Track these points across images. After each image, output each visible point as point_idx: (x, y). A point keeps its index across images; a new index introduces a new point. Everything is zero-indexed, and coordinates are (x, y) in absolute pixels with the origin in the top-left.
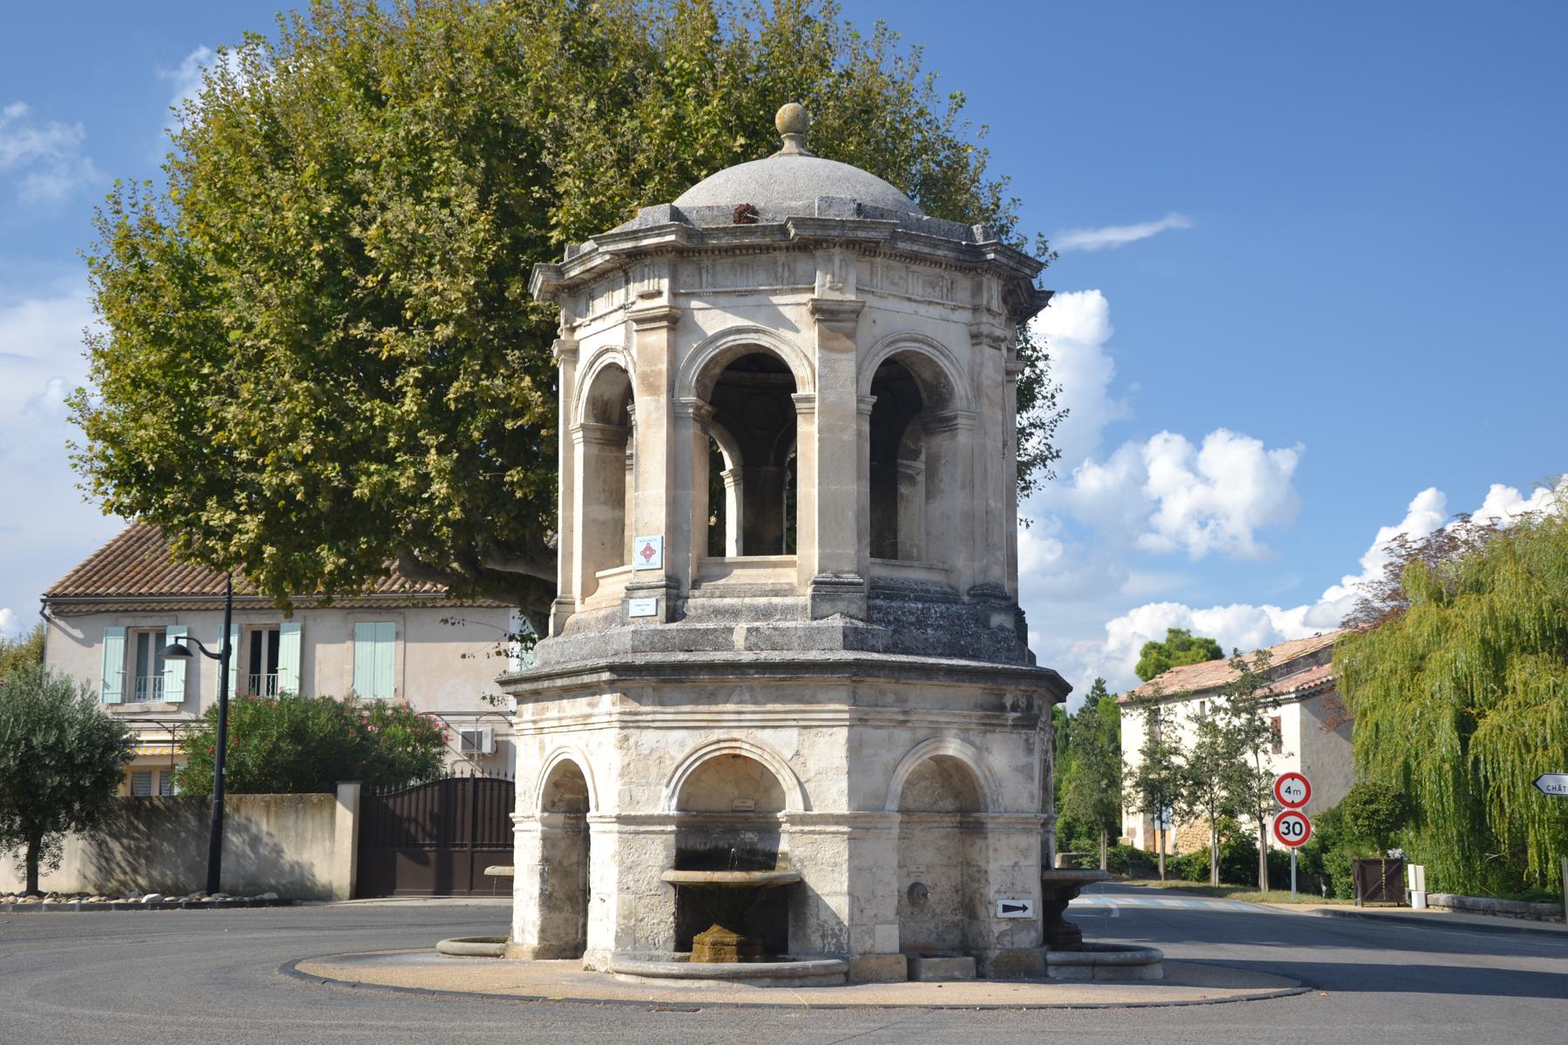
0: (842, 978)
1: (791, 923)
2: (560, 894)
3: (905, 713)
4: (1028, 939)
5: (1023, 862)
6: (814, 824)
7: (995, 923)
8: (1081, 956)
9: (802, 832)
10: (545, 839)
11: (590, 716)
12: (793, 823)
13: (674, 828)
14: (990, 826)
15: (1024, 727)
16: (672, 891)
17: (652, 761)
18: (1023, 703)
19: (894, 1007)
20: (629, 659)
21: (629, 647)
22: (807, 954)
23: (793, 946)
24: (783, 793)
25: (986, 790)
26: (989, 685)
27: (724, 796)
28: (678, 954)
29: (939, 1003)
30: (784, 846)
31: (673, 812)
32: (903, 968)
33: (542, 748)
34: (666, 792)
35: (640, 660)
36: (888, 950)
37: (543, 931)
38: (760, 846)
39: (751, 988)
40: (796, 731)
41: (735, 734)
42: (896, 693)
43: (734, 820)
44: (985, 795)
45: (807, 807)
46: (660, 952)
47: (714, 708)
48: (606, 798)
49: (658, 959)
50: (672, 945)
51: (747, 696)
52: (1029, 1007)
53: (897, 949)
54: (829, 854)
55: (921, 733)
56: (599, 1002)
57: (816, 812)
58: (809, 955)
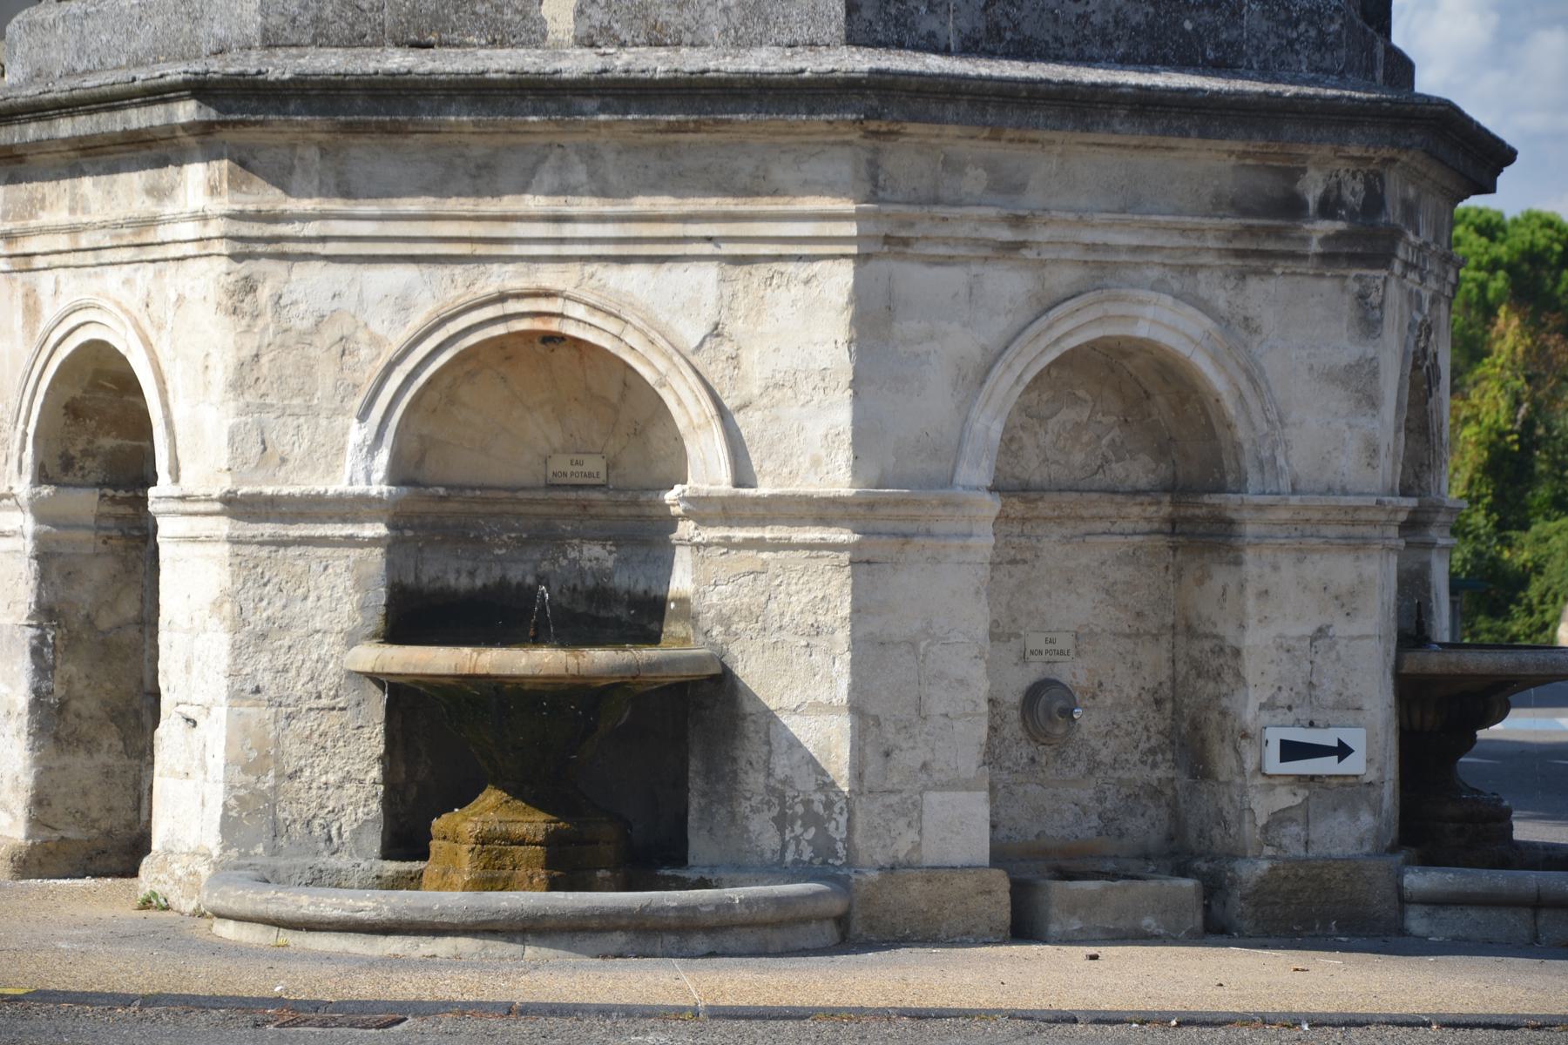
0: (830, 932)
1: (696, 783)
2: (88, 705)
3: (1017, 221)
4: (1349, 834)
5: (1341, 628)
6: (761, 522)
7: (1260, 792)
8: (1501, 880)
9: (728, 544)
10: (45, 556)
11: (152, 222)
12: (702, 521)
13: (380, 530)
14: (1250, 529)
15: (1354, 259)
16: (377, 702)
17: (320, 350)
18: (1354, 192)
19: (941, 1014)
20: (250, 64)
21: (253, 30)
22: (739, 867)
23: (700, 846)
24: (678, 439)
25: (1242, 433)
26: (1257, 144)
27: (521, 446)
28: (392, 867)
29: (1067, 1005)
30: (681, 581)
31: (378, 487)
32: (1000, 906)
33: (32, 310)
34: (358, 434)
35: (281, 67)
36: (958, 857)
37: (40, 801)
38: (622, 581)
39: (572, 959)
40: (711, 271)
41: (548, 277)
42: (991, 167)
43: (555, 511)
44: (1237, 446)
45: (742, 474)
46: (343, 861)
47: (489, 206)
48: (197, 443)
49: (337, 881)
50: (374, 842)
51: (579, 174)
52: (1317, 1022)
53: (982, 853)
54: (800, 601)
55: (1063, 278)
56: (126, 1000)
57: (764, 489)
58: (742, 870)
